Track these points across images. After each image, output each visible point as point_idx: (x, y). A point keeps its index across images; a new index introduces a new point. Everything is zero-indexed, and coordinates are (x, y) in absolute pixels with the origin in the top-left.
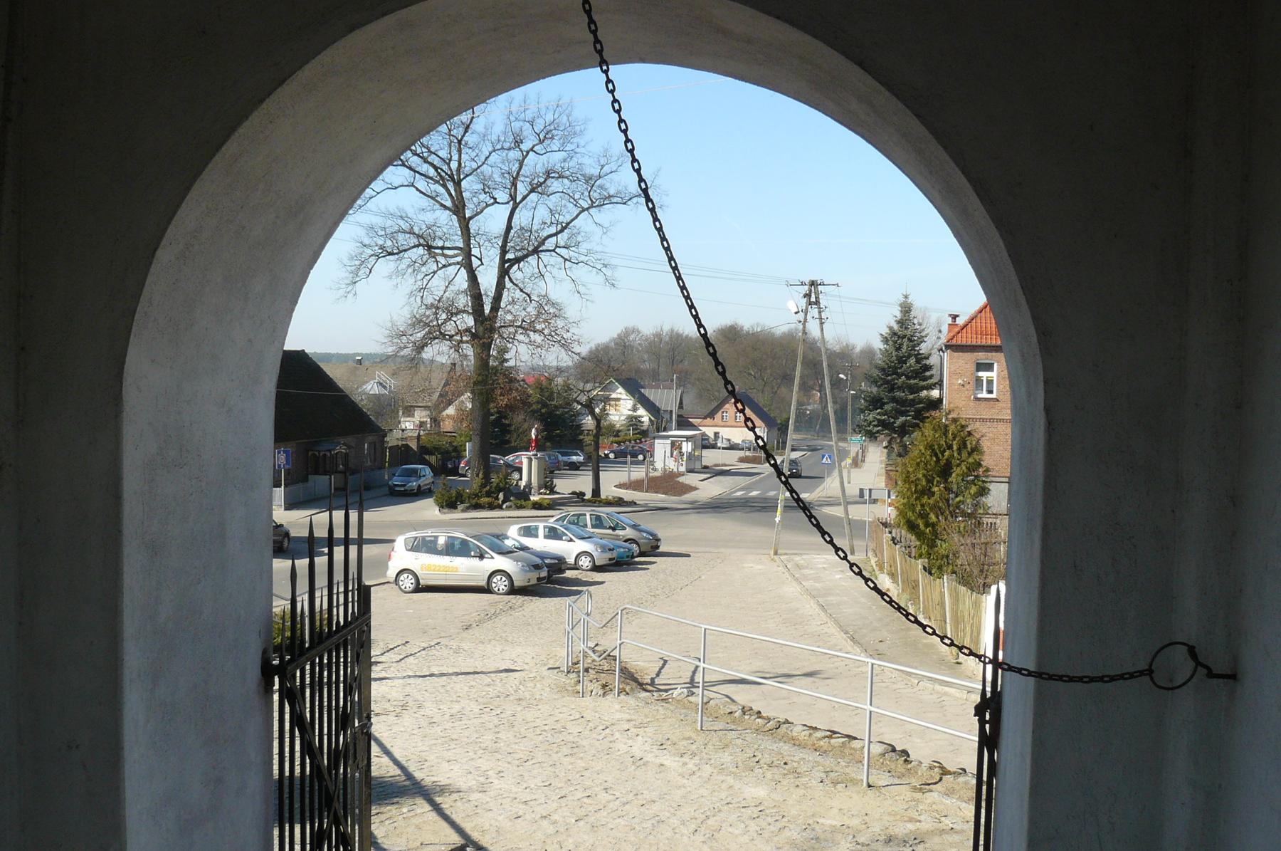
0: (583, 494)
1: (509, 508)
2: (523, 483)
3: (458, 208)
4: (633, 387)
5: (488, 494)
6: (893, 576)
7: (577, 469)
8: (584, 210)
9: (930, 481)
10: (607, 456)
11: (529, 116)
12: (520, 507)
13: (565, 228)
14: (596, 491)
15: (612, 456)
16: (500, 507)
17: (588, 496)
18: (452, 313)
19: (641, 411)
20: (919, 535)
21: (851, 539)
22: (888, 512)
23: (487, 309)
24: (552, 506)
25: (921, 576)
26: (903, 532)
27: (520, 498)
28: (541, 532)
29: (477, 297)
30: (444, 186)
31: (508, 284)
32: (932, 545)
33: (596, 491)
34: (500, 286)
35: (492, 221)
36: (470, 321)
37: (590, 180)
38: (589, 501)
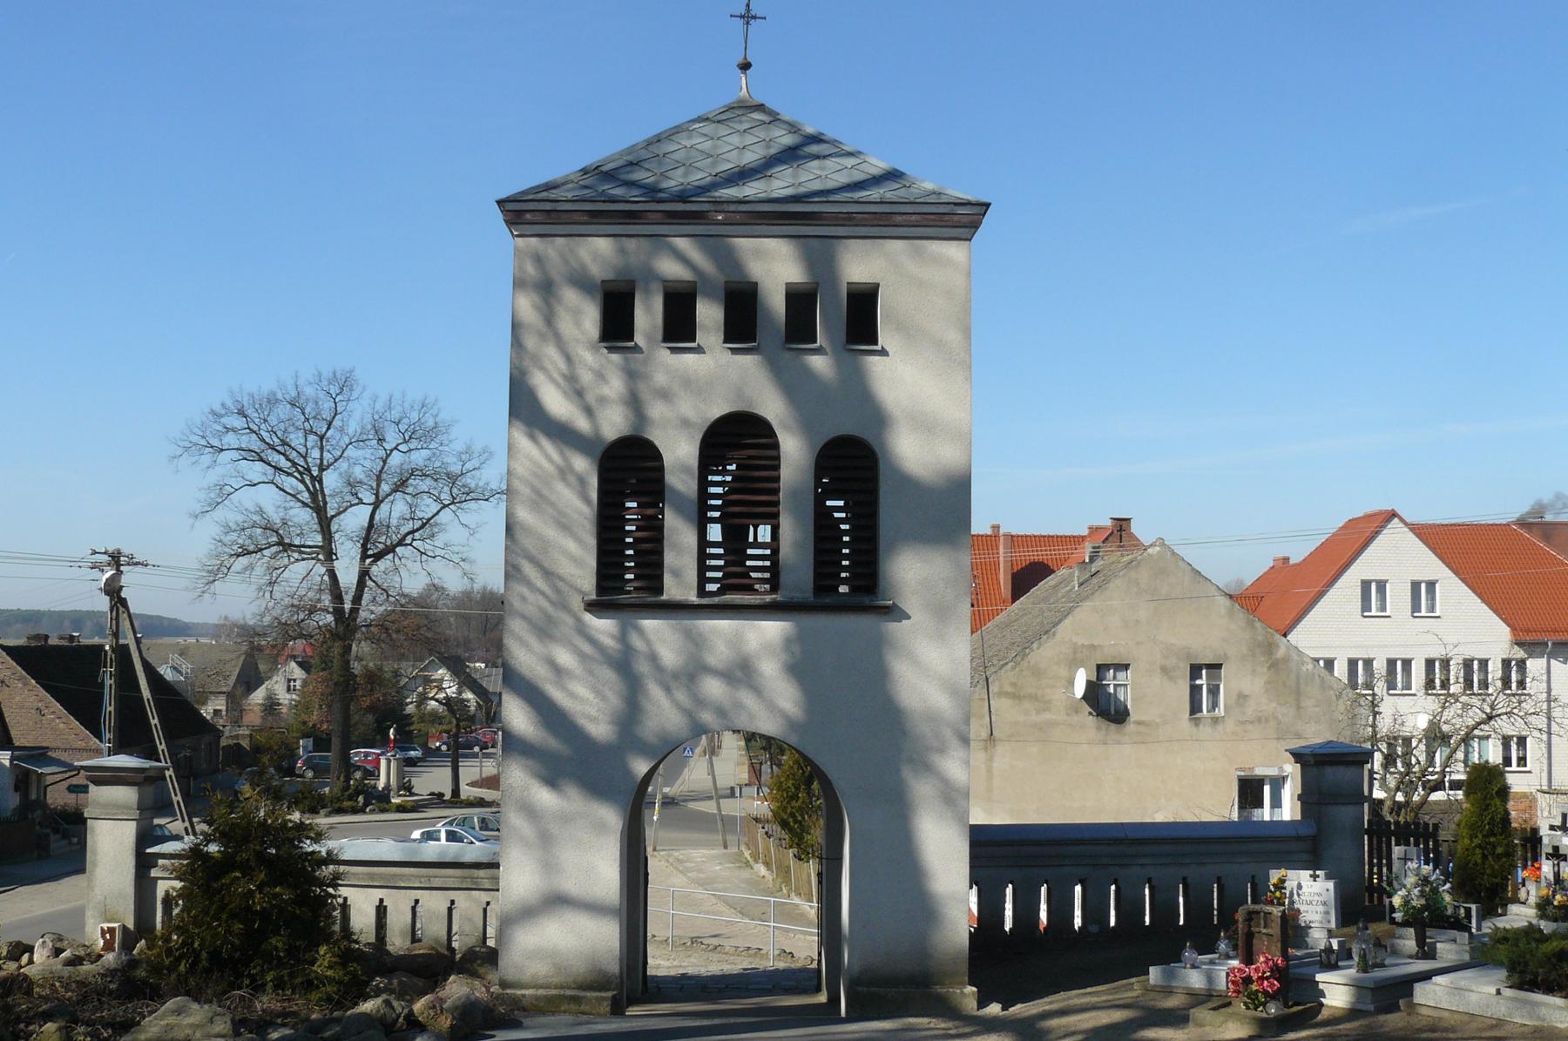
0: (441, 795)
1: (372, 811)
2: (381, 784)
3: (318, 505)
4: (457, 667)
5: (350, 798)
6: (767, 864)
7: (415, 765)
8: (445, 506)
9: (797, 788)
10: (438, 748)
11: (395, 415)
12: (383, 811)
13: (424, 525)
14: (456, 792)
15: (444, 748)
16: (362, 811)
17: (448, 797)
18: (312, 610)
19: (468, 695)
20: (791, 830)
21: (724, 835)
22: (760, 806)
23: (347, 606)
24: (416, 808)
25: (792, 862)
26: (777, 828)
27: (380, 800)
28: (443, 835)
29: (337, 596)
30: (303, 482)
31: (369, 583)
32: (801, 838)
33: (456, 792)
34: (361, 584)
35: (354, 521)
36: (330, 618)
37: (453, 479)
38: (449, 802)
